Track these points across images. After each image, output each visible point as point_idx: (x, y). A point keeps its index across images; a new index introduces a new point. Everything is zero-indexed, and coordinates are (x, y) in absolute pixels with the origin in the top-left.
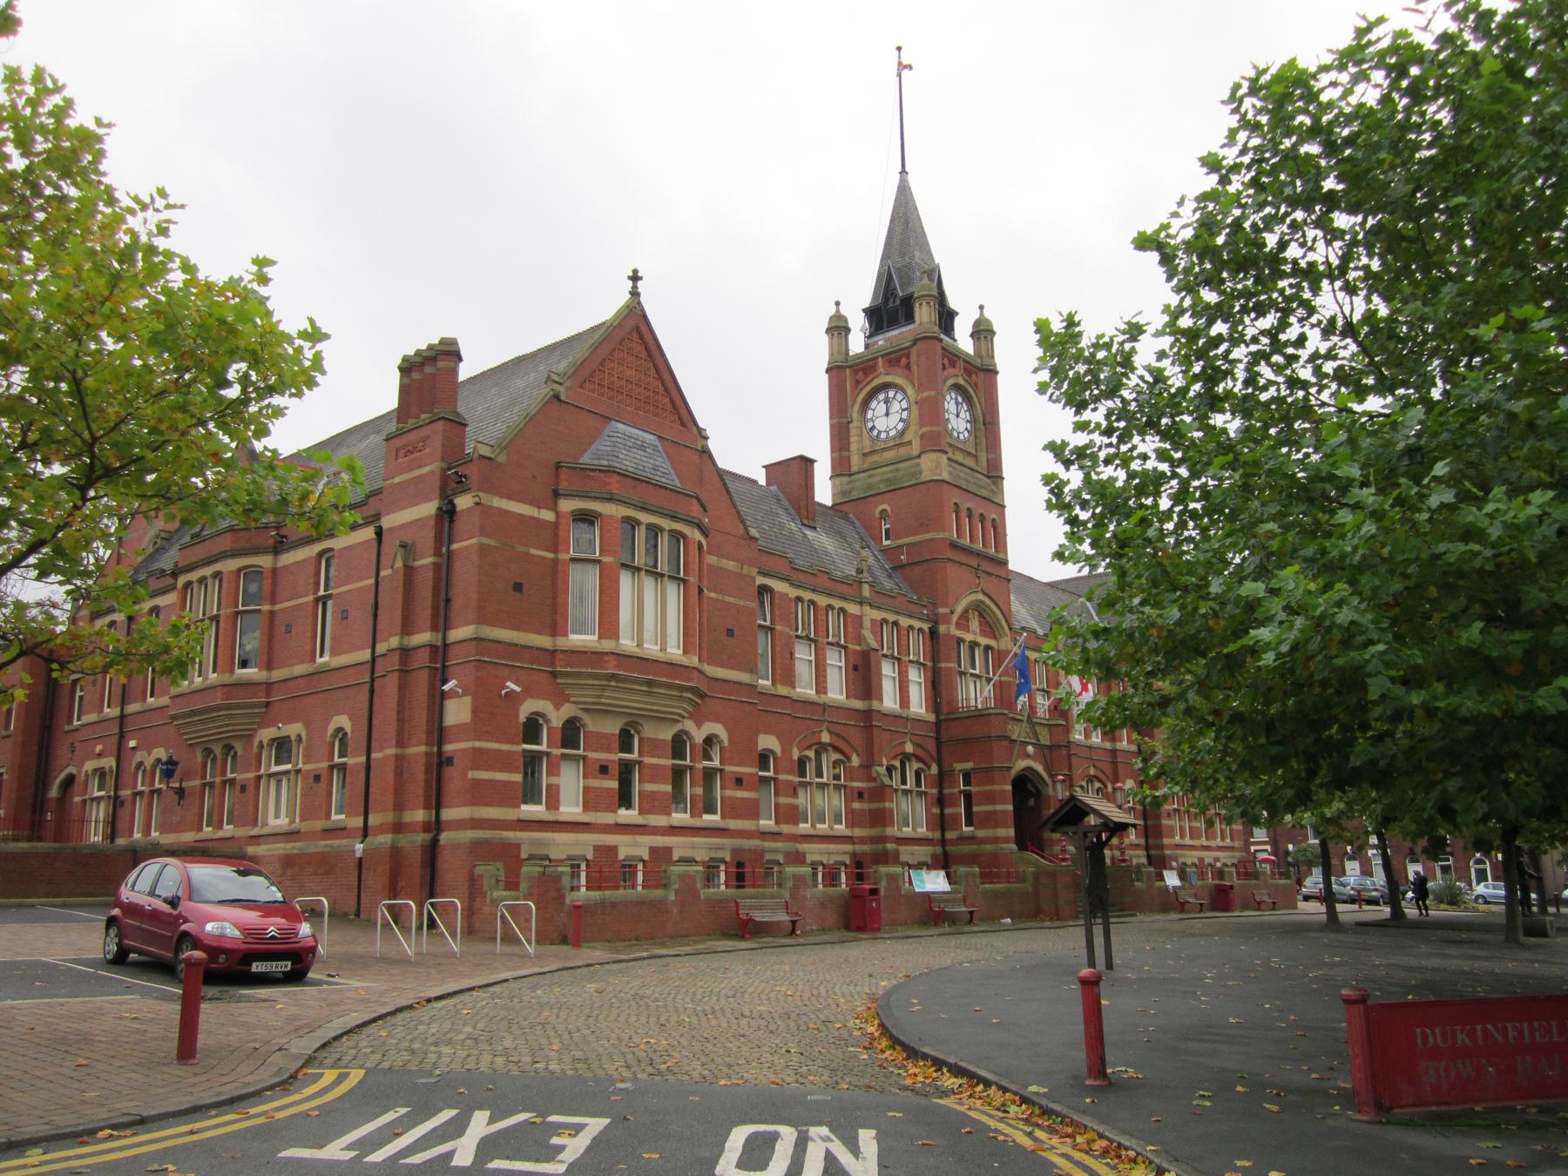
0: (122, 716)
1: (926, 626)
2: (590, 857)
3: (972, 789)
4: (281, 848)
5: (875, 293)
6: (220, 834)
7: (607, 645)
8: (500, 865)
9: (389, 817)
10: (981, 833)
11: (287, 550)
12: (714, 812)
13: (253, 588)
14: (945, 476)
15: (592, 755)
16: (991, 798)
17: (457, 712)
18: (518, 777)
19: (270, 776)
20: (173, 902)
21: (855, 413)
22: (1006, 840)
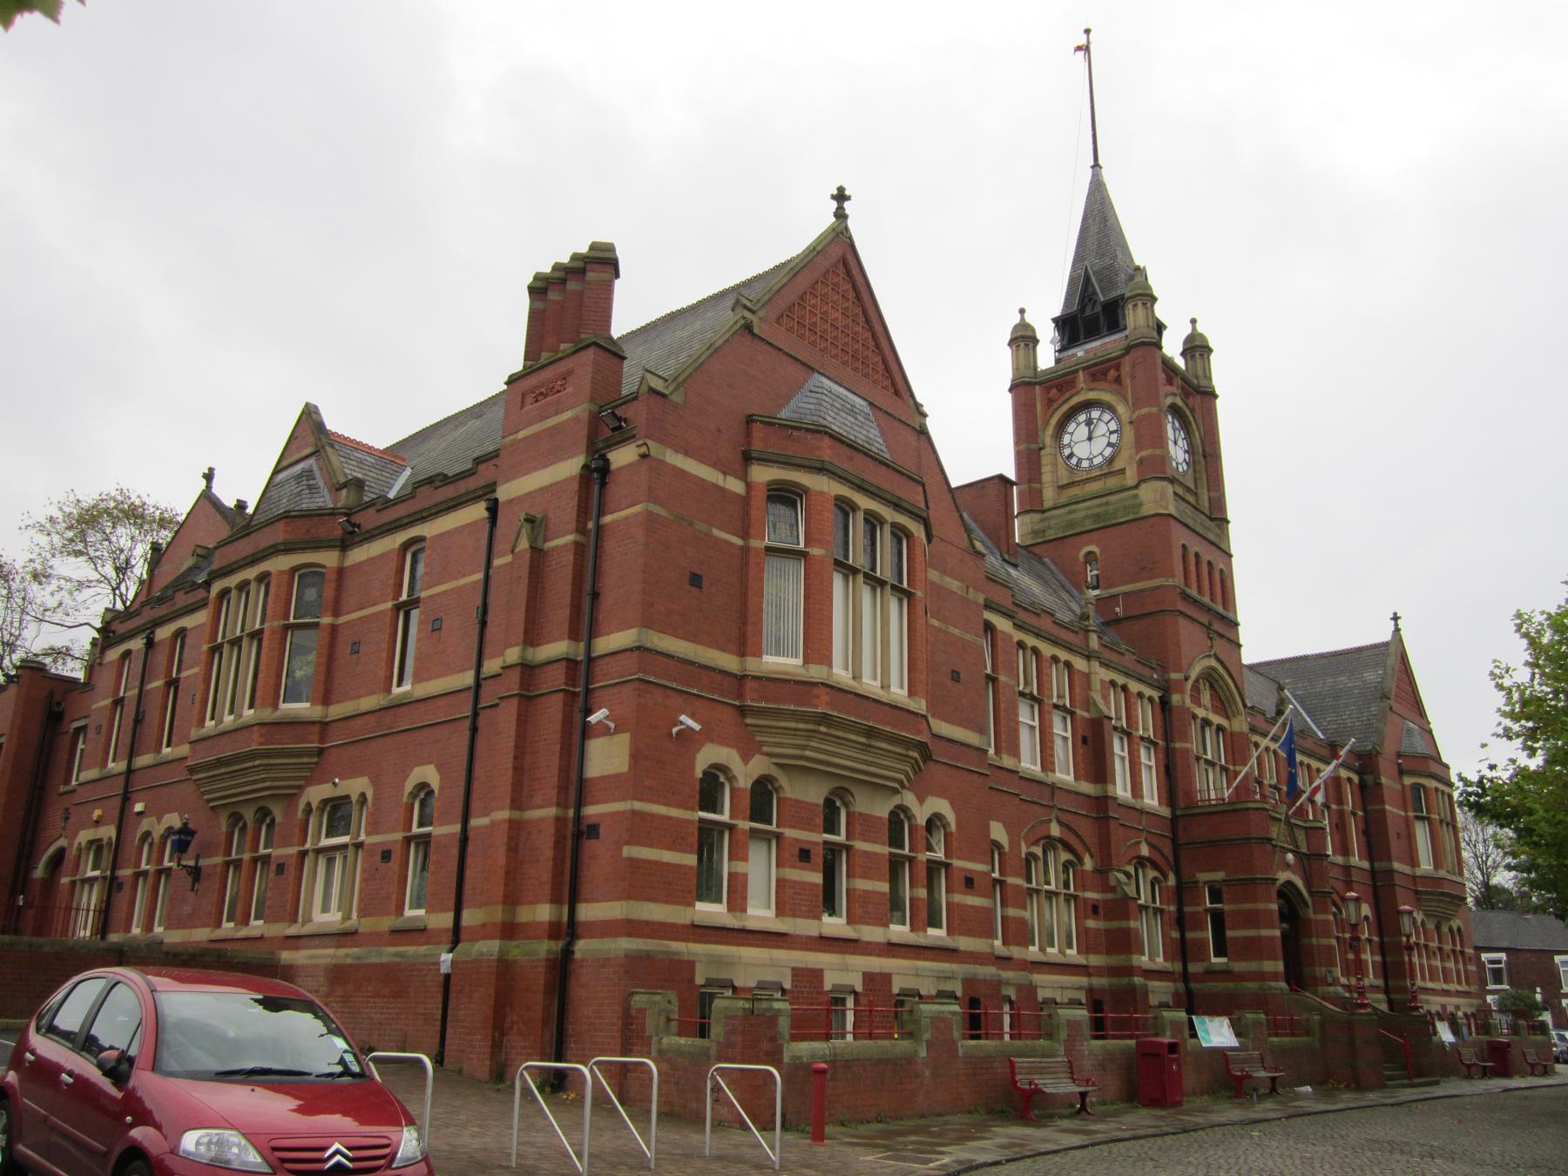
0: (130, 771)
1: (1156, 695)
2: (859, 988)
3: (1226, 907)
4: (327, 955)
5: (1067, 299)
6: (244, 932)
7: (816, 673)
8: (673, 996)
9: (497, 914)
10: (1239, 966)
11: (360, 543)
12: (938, 925)
13: (311, 594)
14: (1172, 510)
15: (790, 833)
16: (1253, 919)
17: (607, 757)
18: (691, 860)
19: (318, 851)
20: (119, 1069)
21: (1048, 436)
22: (1274, 976)
